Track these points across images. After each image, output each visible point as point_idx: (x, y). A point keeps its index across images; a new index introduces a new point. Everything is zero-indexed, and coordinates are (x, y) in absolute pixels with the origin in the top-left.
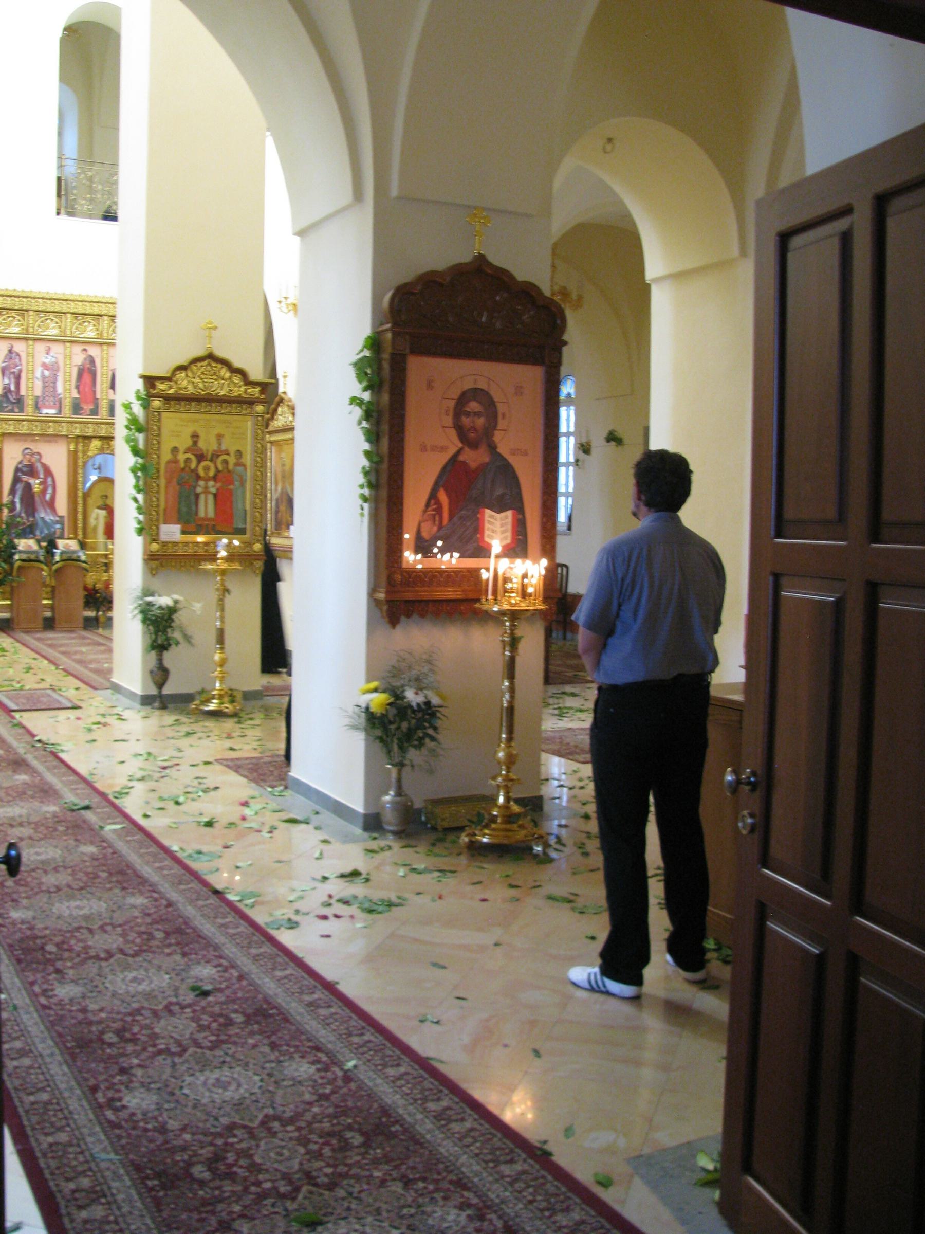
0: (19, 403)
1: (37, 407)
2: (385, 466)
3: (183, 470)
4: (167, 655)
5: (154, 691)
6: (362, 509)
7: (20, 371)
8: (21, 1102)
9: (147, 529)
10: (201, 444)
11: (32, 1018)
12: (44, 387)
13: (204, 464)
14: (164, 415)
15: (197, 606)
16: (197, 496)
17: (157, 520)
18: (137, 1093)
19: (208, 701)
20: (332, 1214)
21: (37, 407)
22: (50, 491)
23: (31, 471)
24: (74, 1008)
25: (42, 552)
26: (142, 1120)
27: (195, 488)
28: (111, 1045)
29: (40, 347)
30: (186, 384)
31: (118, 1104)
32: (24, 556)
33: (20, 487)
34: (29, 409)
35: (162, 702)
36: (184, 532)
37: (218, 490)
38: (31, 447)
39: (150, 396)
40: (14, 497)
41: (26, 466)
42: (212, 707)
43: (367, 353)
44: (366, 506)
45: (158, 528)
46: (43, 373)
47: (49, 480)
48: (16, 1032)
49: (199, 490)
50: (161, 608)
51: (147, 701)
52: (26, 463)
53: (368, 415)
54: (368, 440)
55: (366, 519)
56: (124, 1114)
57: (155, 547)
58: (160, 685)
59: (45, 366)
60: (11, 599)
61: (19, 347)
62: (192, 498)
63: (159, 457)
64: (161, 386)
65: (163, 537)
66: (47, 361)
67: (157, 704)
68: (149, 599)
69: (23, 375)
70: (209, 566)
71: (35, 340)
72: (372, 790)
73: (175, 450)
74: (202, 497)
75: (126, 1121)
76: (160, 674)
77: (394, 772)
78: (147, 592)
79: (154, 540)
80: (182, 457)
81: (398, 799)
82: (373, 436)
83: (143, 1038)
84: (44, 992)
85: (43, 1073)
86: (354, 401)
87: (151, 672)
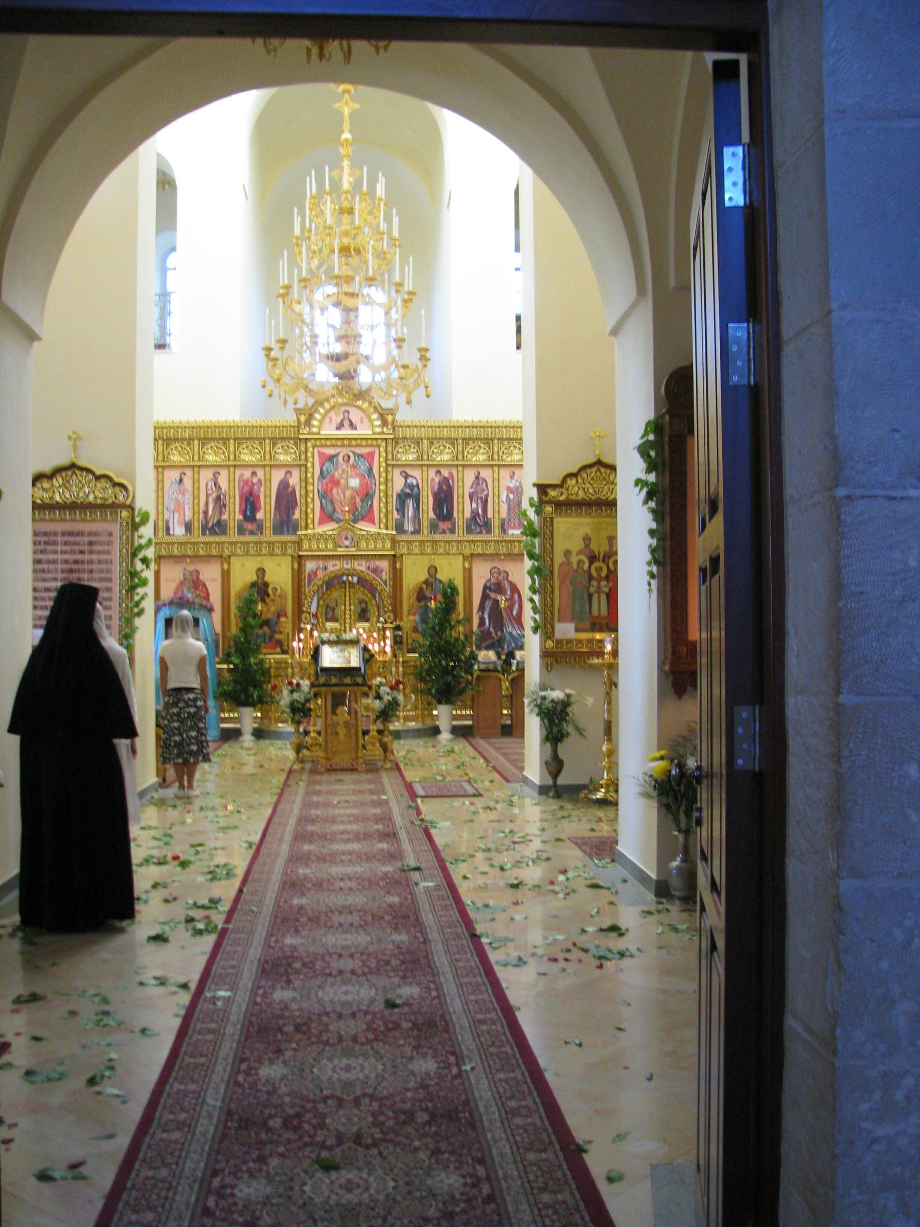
0: (487, 526)
1: (503, 530)
2: (668, 544)
3: (576, 571)
4: (560, 747)
5: (549, 781)
6: (649, 584)
7: (487, 495)
9: (545, 628)
10: (593, 546)
12: (509, 509)
13: (596, 564)
14: (555, 520)
15: (590, 700)
16: (590, 596)
17: (552, 619)
18: (446, 1188)
19: (597, 790)
21: (503, 530)
22: (517, 606)
23: (499, 589)
25: (499, 663)
27: (588, 589)
29: (505, 473)
30: (575, 490)
31: (469, 1180)
32: (483, 667)
33: (488, 604)
34: (496, 530)
35: (556, 791)
36: (577, 630)
37: (610, 590)
38: (499, 566)
39: (541, 502)
40: (483, 613)
41: (494, 584)
42: (600, 795)
43: (651, 437)
44: (654, 583)
45: (553, 627)
46: (507, 496)
47: (516, 596)
48: (520, 1135)
49: (592, 590)
50: (553, 701)
51: (543, 790)
52: (493, 580)
53: (650, 496)
54: (655, 520)
55: (654, 595)
56: (467, 1169)
57: (550, 644)
58: (555, 775)
59: (509, 489)
60: (472, 708)
61: (486, 474)
62: (586, 598)
63: (552, 560)
64: (552, 493)
65: (558, 635)
66: (511, 485)
67: (551, 794)
68: (543, 693)
69: (490, 499)
70: (596, 661)
71: (499, 466)
72: (663, 859)
73: (567, 553)
74: (595, 596)
76: (555, 766)
77: (681, 838)
78: (543, 687)
79: (549, 638)
80: (574, 559)
81: (683, 865)
82: (658, 514)
85: (529, 1182)
86: (638, 482)
87: (546, 763)
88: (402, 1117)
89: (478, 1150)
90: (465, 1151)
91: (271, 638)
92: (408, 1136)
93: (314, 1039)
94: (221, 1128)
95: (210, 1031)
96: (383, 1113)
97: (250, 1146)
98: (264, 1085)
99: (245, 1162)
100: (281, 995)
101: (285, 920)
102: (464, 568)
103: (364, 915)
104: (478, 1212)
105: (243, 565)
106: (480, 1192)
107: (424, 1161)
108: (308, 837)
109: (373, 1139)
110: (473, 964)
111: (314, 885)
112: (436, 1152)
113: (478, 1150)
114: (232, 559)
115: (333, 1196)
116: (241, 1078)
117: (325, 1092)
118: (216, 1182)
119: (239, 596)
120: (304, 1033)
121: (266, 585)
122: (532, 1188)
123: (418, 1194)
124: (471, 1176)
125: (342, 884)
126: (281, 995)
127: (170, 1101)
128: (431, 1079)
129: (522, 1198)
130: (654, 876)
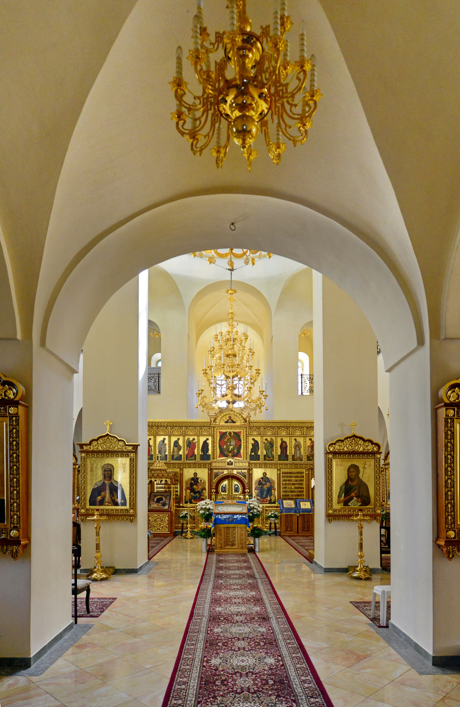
8: (311, 677)
11: (284, 653)
18: (270, 662)
20: (248, 700)
24: (270, 654)
26: (283, 701)
28: (272, 679)
31: (276, 660)
48: (299, 670)
64: (85, 448)
75: (276, 656)
83: (259, 680)
84: (270, 630)
85: (298, 673)
88: (257, 644)
89: (279, 653)
90: (288, 697)
91: (199, 498)
92: (253, 622)
93: (230, 689)
94: (205, 645)
95: (193, 645)
96: (257, 680)
97: (214, 650)
98: (216, 634)
99: (209, 698)
100: (218, 609)
101: (216, 600)
102: (278, 474)
103: (243, 599)
104: (279, 668)
105: (188, 472)
106: (280, 664)
107: (274, 700)
108: (221, 568)
109: (254, 690)
110: (275, 601)
111: (224, 601)
112: (278, 696)
113: (279, 653)
114: (184, 469)
115: (238, 663)
116: (205, 664)
117: (235, 670)
118: (205, 659)
119: (187, 483)
120: (226, 646)
121: (198, 479)
122: (294, 663)
123: (262, 664)
124: (277, 659)
125: (234, 576)
126: (218, 609)
127: (189, 638)
128: (265, 633)
129: (296, 677)
130: (431, 652)
